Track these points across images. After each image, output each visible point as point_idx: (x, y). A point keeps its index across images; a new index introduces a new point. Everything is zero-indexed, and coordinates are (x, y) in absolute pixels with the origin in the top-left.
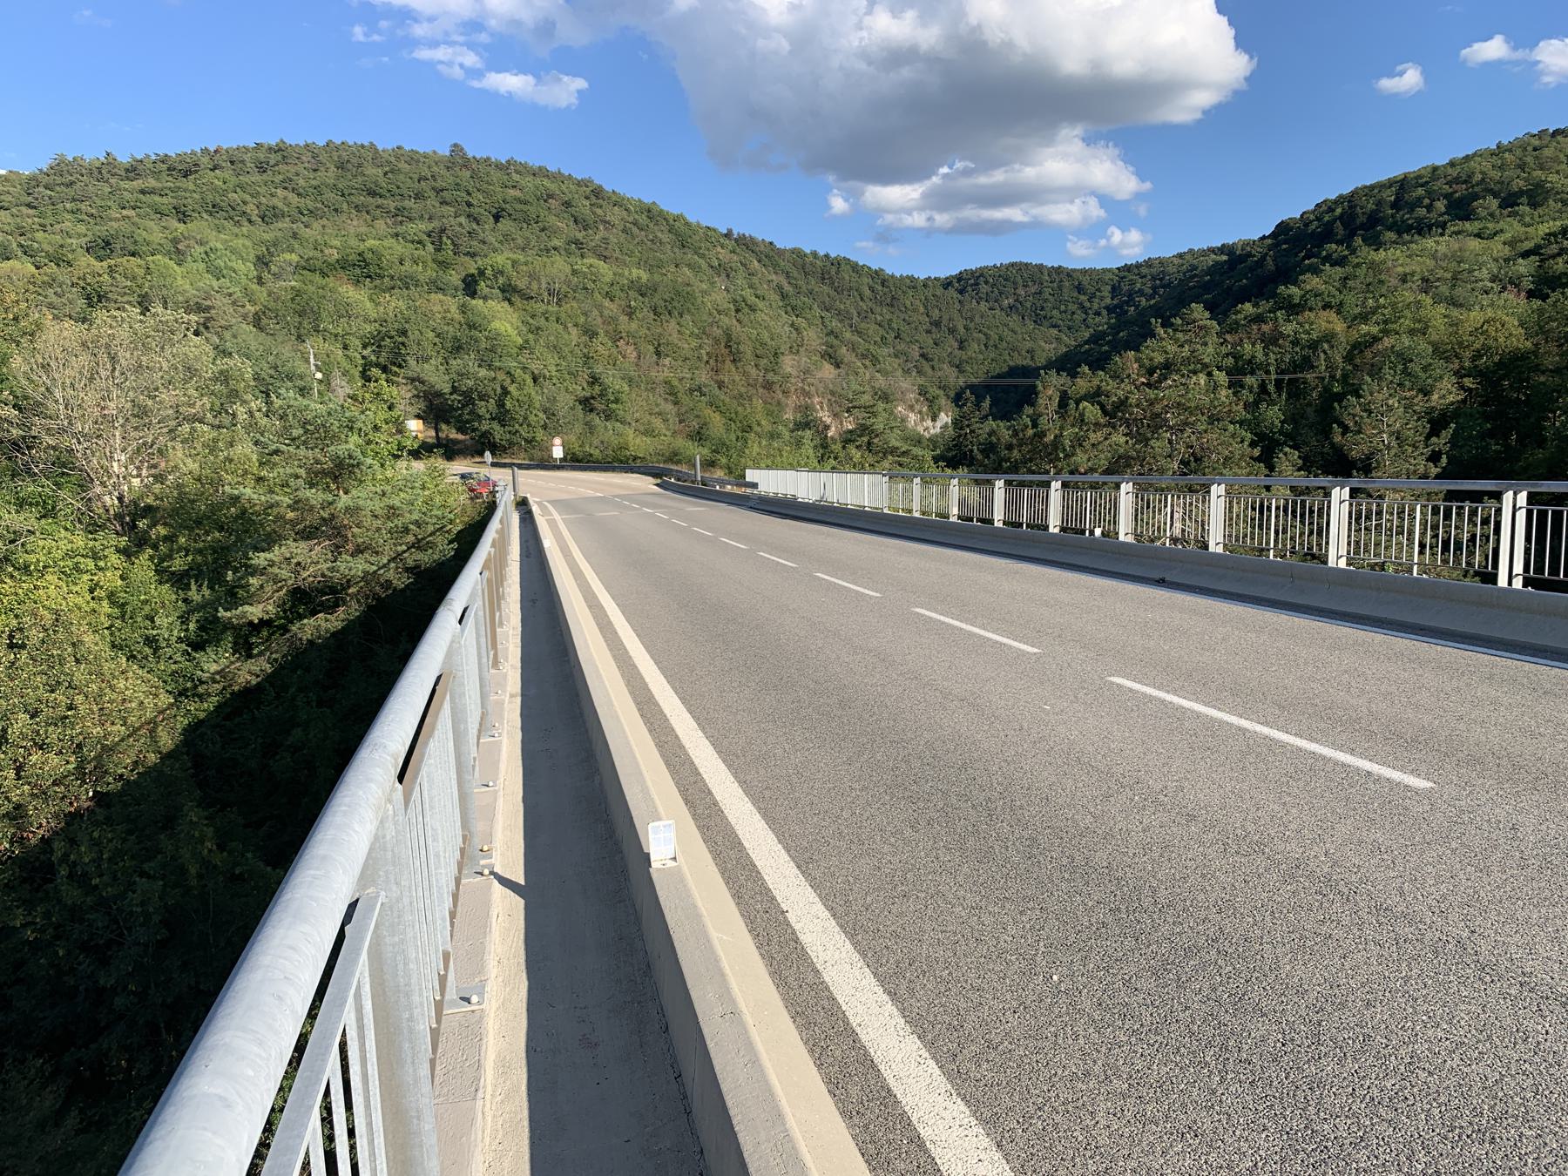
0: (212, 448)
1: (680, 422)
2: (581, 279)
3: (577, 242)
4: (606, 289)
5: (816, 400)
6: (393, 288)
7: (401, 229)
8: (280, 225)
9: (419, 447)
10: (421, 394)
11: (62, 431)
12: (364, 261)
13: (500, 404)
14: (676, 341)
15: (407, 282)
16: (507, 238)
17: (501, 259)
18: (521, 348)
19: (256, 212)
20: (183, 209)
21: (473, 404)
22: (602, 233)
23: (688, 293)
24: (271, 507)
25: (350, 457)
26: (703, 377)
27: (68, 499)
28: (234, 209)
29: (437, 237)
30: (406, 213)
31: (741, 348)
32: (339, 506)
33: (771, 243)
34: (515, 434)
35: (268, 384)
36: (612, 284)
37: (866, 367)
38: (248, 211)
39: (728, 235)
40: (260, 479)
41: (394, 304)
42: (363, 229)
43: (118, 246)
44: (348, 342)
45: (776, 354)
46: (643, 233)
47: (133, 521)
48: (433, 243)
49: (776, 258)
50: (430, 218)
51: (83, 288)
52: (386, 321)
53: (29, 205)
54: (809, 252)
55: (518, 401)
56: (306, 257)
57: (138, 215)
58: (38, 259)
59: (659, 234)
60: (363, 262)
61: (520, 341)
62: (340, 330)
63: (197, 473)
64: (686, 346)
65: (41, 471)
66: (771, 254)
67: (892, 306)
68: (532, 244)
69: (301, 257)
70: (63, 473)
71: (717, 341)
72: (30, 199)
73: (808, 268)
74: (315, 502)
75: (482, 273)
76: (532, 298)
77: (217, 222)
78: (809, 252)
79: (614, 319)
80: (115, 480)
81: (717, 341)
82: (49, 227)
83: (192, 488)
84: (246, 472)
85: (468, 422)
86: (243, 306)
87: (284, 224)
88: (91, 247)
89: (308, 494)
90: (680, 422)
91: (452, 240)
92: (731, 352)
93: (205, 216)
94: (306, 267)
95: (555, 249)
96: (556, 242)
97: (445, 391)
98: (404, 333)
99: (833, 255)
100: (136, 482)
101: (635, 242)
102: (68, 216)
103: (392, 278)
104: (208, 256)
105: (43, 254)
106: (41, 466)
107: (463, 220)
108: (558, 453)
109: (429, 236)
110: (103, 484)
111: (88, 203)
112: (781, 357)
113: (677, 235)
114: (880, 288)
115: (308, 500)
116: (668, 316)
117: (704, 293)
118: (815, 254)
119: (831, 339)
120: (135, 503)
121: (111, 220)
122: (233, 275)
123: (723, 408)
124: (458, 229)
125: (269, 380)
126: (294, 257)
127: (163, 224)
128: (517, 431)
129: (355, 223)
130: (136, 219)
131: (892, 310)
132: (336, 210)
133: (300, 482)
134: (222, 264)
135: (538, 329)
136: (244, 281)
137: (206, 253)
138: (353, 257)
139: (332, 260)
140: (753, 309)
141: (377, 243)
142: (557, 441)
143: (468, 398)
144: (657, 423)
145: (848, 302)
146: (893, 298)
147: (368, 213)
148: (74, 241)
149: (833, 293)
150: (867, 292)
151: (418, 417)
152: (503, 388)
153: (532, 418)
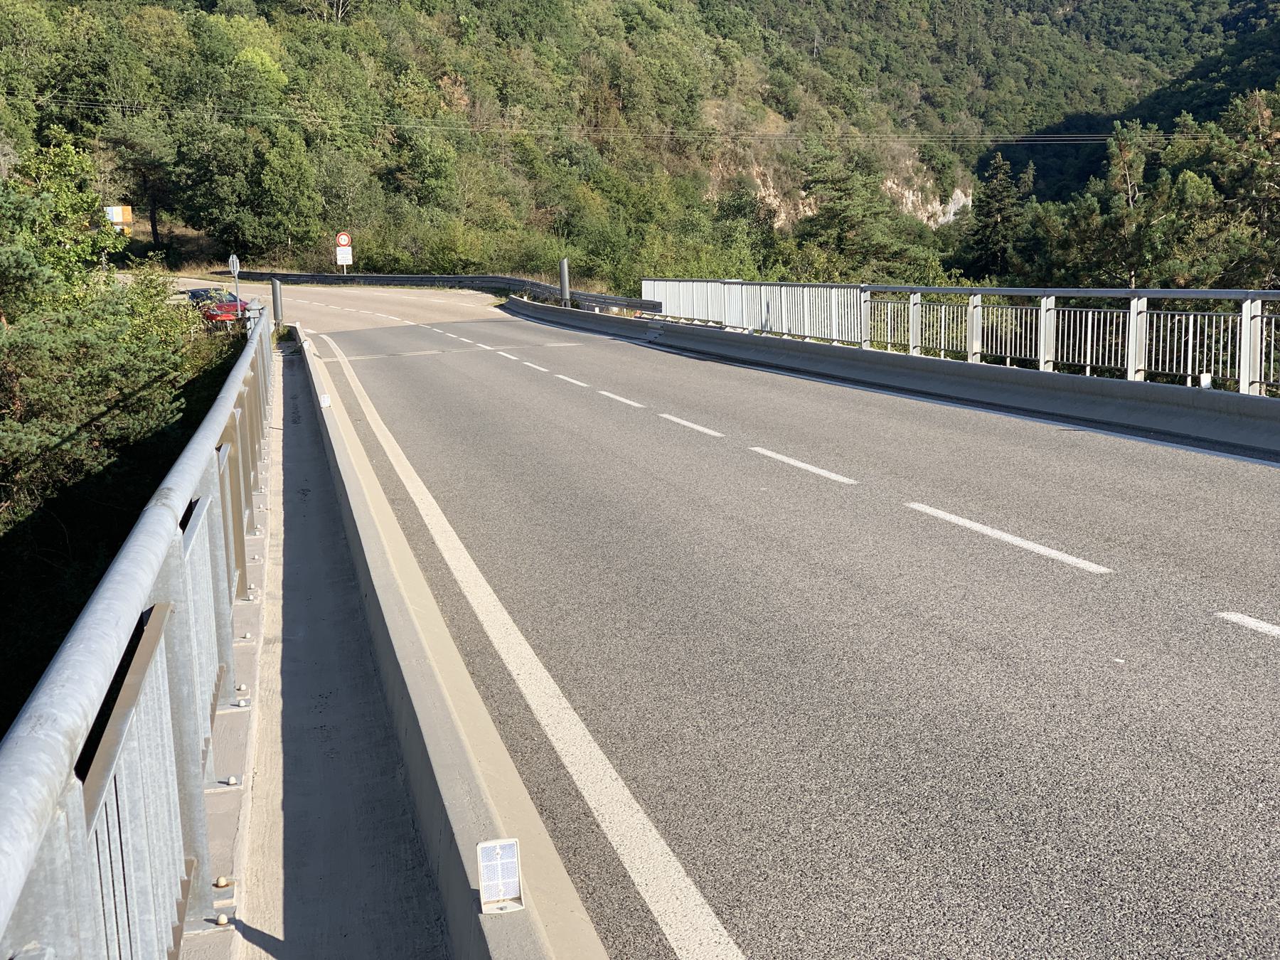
9: (125, 249)
10: (130, 165)
13: (254, 180)
14: (532, 79)
18: (287, 91)
21: (211, 181)
25: (19, 265)
26: (575, 134)
31: (636, 89)
34: (276, 227)
37: (835, 117)
44: (15, 83)
45: (691, 97)
52: (74, 50)
55: (281, 174)
64: (548, 85)
67: (878, 19)
76: (303, 11)
81: (596, 77)
92: (619, 94)
97: (167, 160)
98: (102, 68)
108: (344, 256)
112: (700, 103)
116: (519, 39)
123: (606, 184)
131: (878, 25)
135: (313, 60)
140: (654, 26)
144: (502, 209)
145: (807, 14)
151: (124, 201)
152: (258, 154)
153: (304, 202)
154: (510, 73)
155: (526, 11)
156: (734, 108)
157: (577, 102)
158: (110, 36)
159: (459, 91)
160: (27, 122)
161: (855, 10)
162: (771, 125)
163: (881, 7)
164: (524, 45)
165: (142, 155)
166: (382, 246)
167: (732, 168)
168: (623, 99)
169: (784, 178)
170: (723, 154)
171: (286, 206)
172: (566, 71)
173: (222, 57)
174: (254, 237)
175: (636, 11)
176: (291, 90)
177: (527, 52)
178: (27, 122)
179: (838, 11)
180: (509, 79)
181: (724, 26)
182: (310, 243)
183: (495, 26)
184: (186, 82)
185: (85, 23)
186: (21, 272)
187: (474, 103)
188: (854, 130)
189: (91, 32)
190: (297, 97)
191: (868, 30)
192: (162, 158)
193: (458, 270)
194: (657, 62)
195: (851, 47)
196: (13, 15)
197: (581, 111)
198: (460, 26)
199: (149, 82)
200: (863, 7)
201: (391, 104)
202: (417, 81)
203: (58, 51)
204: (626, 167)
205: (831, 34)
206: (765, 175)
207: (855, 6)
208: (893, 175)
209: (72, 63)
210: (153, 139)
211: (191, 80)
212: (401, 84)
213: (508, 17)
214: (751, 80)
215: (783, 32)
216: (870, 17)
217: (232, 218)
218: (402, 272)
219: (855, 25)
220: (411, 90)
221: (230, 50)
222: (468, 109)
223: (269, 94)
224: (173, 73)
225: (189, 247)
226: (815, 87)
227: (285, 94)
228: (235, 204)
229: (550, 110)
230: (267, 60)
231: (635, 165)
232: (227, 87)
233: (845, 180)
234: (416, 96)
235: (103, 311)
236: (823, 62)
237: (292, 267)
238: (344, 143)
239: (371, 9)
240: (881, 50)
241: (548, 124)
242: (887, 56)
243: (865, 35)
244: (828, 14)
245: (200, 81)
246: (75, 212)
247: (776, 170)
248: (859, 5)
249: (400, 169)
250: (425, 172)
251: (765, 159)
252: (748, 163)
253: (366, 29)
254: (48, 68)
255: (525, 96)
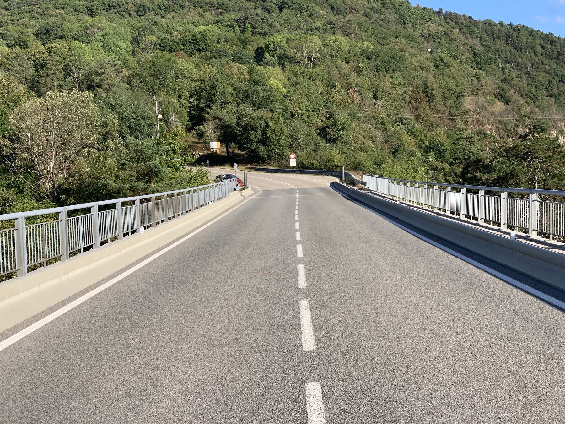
0: (97, 161)
1: (386, 142)
2: (329, 50)
3: (331, 24)
4: (345, 55)
5: (487, 127)
6: (211, 58)
7: (220, 18)
8: (147, 17)
9: (195, 162)
10: (219, 127)
11: (29, 151)
12: (196, 40)
13: (264, 133)
14: (388, 89)
15: (220, 54)
16: (286, 23)
17: (279, 38)
18: (285, 96)
19: (133, 9)
20: (91, 8)
21: (248, 133)
22: (349, 16)
23: (400, 57)
24: (121, 189)
25: (156, 167)
26: (406, 114)
27: (29, 185)
28: (121, 7)
29: (242, 22)
30: (224, 8)
31: (434, 93)
32: (150, 190)
33: (470, 17)
34: (271, 151)
35: (131, 122)
36: (349, 52)
37: (528, 104)
38: (129, 8)
39: (439, 13)
40: (118, 177)
41: (209, 70)
42: (197, 18)
43: (53, 33)
44: (181, 93)
45: (459, 96)
46: (377, 15)
47: (58, 196)
48: (240, 26)
49: (473, 27)
50: (239, 10)
51: (33, 61)
52: (204, 81)
53: (5, 9)
54: (497, 22)
55: (274, 131)
56: (161, 38)
57: (66, 13)
58: (9, 41)
59: (388, 16)
60: (196, 41)
61: (285, 91)
62: (177, 86)
63: (89, 172)
64: (395, 92)
65: (18, 170)
66: (470, 24)
67: (558, 59)
68: (302, 25)
69: (159, 38)
70: (28, 172)
71: (417, 88)
72: (6, 4)
73: (497, 34)
74: (139, 188)
75: (267, 46)
76: (297, 62)
77: (110, 15)
78: (497, 22)
79: (348, 76)
80: (51, 175)
81: (417, 88)
82: (16, 22)
83: (87, 180)
84: (112, 173)
85: (245, 143)
86: (122, 72)
87: (150, 16)
88: (38, 33)
89: (136, 184)
90: (386, 142)
91: (251, 24)
92: (427, 95)
93: (104, 12)
94: (162, 46)
95: (316, 28)
96: (318, 24)
97: (233, 125)
98: (214, 87)
99: (515, 24)
100: (61, 176)
101: (371, 21)
102: (26, 14)
103: (211, 52)
104: (104, 38)
105: (12, 38)
106: (19, 168)
107: (259, 11)
108: (293, 163)
109: (238, 22)
110: (46, 178)
111: (38, 6)
112: (463, 99)
113: (401, 15)
114: (549, 46)
115: (136, 186)
116: (385, 73)
117: (413, 55)
118: (501, 24)
119: (504, 85)
120: (60, 187)
121: (50, 16)
122: (118, 49)
123: (416, 133)
124: (255, 17)
125: (131, 120)
126: (154, 38)
127: (80, 18)
128: (273, 149)
129: (192, 14)
130: (64, 15)
131: (558, 62)
132: (181, 6)
133: (133, 178)
134: (112, 43)
135: (297, 83)
136: (124, 54)
137: (103, 36)
138: (190, 38)
139: (176, 39)
140: (446, 65)
141: (205, 28)
142: (293, 156)
143: (245, 128)
144: (369, 143)
145: (525, 57)
146: (559, 53)
147: (201, 7)
148: (29, 30)
149: (514, 50)
150: (539, 50)
151: (219, 140)
152: (266, 123)
153: (282, 141)
154: (379, 87)
155: (389, 61)
156: (480, 100)
157: (408, 99)
158: (218, 75)
159: (356, 94)
160: (185, 108)
161: (548, 55)
162: (497, 107)
163: (560, 54)
164: (387, 75)
165: (224, 123)
166: (308, 159)
167: (477, 126)
168: (428, 97)
169: (501, 131)
170: (473, 120)
171: (275, 143)
172: (404, 86)
173: (261, 83)
174: (263, 154)
175: (440, 59)
176: (287, 96)
177: (387, 78)
178: (185, 108)
179: (540, 55)
180: (378, 89)
181: (480, 64)
182: (284, 157)
183: (376, 67)
184: (246, 93)
185: (209, 70)
186: (156, 169)
187: (362, 99)
188: (536, 110)
189: (211, 73)
190: (289, 98)
191: (553, 64)
192: (231, 124)
193: (334, 169)
194: (445, 82)
195: (545, 72)
196: (182, 67)
197: (410, 102)
198: (359, 68)
199: (231, 93)
200: (551, 54)
201: (327, 100)
202: (339, 91)
203: (198, 81)
204: (428, 126)
205: (535, 66)
206: (492, 129)
207: (548, 53)
208: (554, 129)
209: (203, 86)
210: (229, 117)
211: (248, 92)
212: (333, 92)
213: (381, 64)
214: (489, 88)
215: (513, 65)
216: (554, 58)
217: (255, 147)
218: (314, 169)
219: (547, 62)
220: (337, 95)
221: (264, 80)
222: (360, 102)
223: (278, 97)
224: (241, 89)
225: (241, 158)
226: (520, 91)
227: (285, 97)
228: (257, 142)
229: (395, 102)
230: (278, 84)
231: (432, 125)
232: (262, 95)
233: (471, 138)
234: (338, 97)
235: (182, 181)
236: (531, 78)
237: (276, 166)
238: (306, 117)
239: (324, 61)
240: (559, 73)
241: (394, 108)
242: (562, 75)
243: (552, 66)
244: (534, 57)
245: (252, 93)
246: (180, 149)
247: (497, 127)
248: (550, 53)
249: (328, 127)
250: (338, 128)
251: (492, 122)
252: (484, 124)
253: (320, 70)
254: (194, 87)
255: (385, 96)
